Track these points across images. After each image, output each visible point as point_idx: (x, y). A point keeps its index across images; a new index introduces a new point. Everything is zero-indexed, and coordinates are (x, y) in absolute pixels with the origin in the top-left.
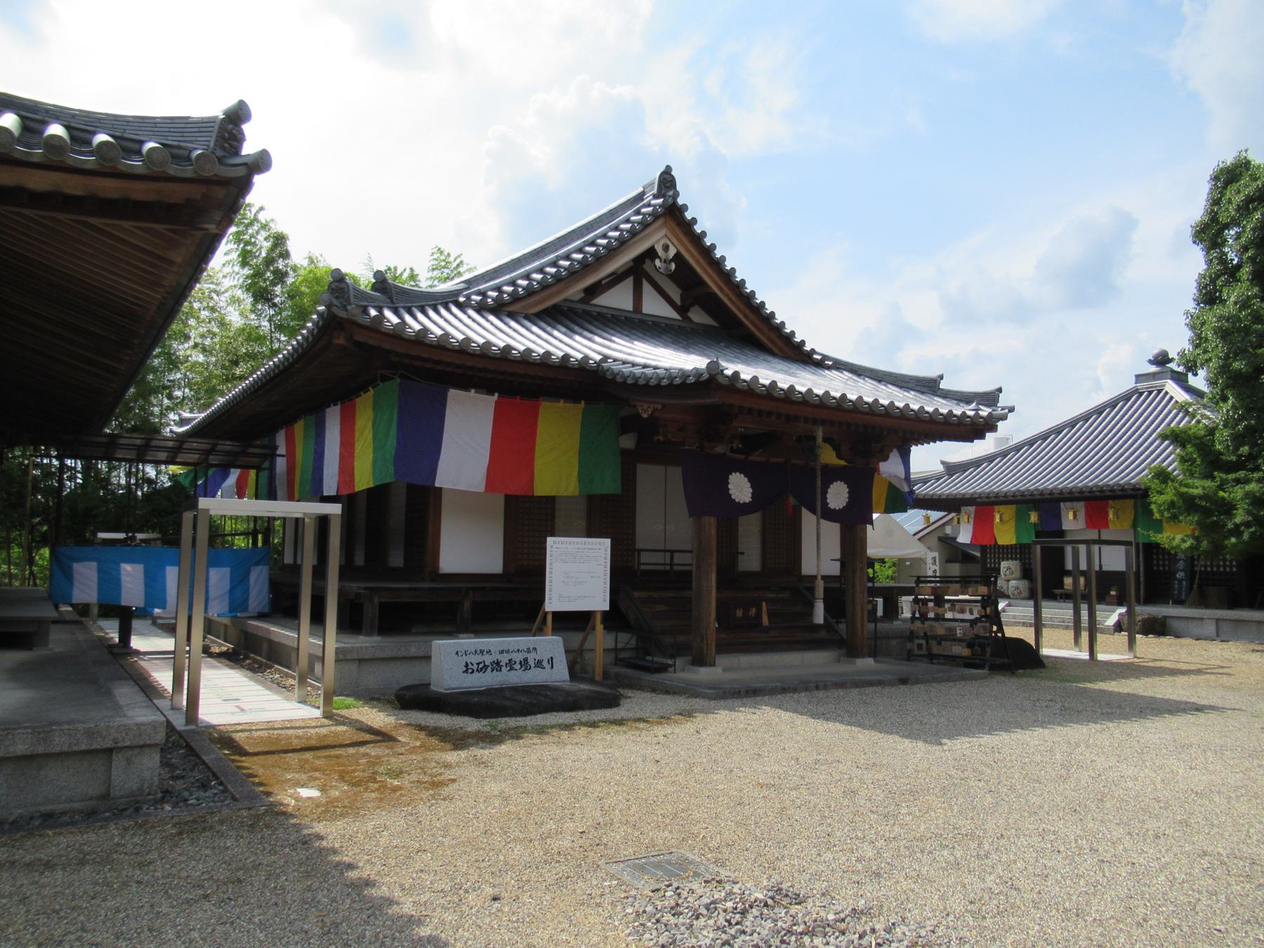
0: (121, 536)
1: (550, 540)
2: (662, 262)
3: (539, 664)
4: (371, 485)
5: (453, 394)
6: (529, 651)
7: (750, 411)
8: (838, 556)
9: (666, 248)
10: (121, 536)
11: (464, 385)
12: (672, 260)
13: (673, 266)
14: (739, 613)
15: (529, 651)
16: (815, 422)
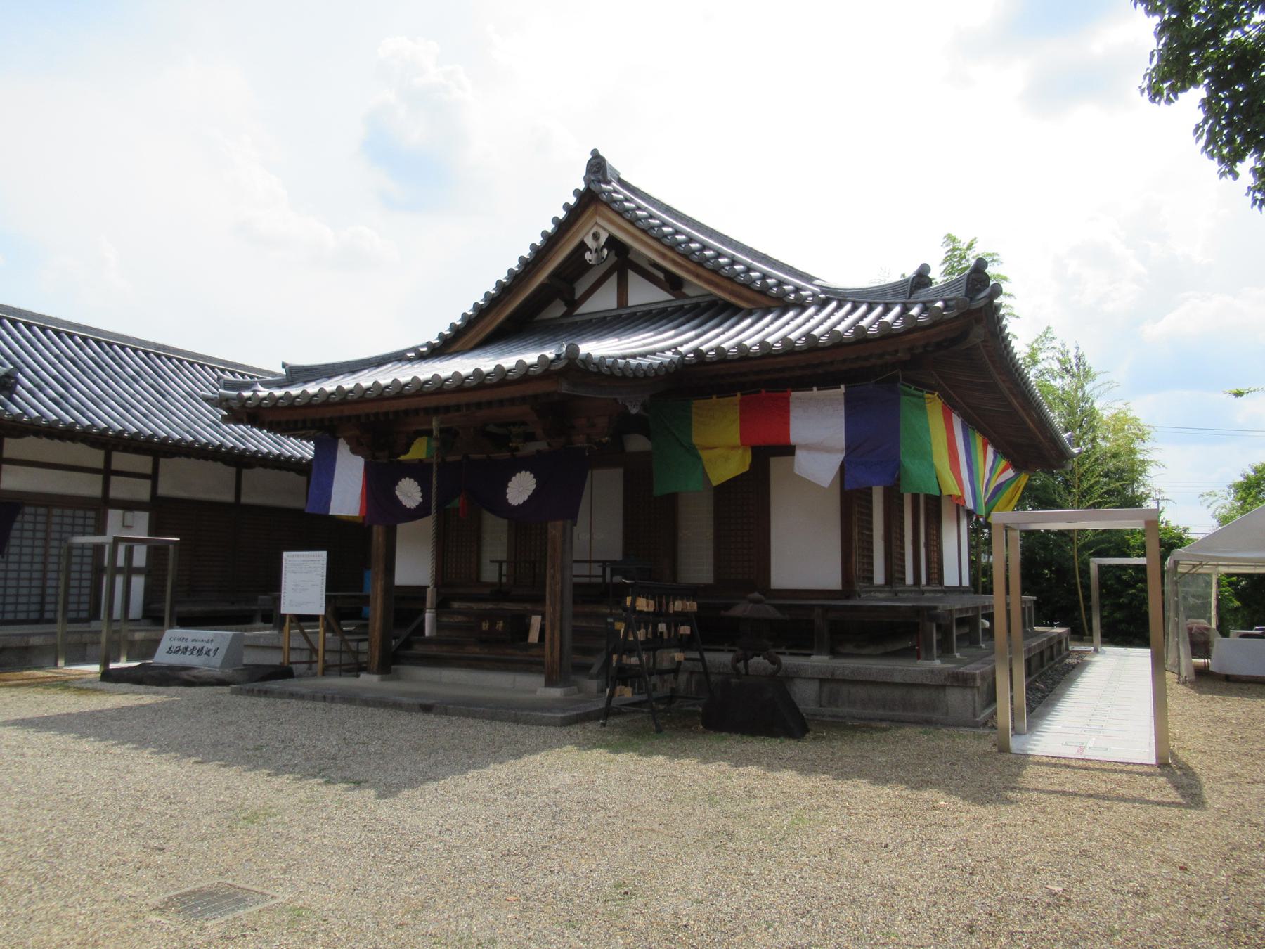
2: (602, 249)
3: (207, 653)
5: (794, 394)
9: (596, 237)
14: (485, 626)
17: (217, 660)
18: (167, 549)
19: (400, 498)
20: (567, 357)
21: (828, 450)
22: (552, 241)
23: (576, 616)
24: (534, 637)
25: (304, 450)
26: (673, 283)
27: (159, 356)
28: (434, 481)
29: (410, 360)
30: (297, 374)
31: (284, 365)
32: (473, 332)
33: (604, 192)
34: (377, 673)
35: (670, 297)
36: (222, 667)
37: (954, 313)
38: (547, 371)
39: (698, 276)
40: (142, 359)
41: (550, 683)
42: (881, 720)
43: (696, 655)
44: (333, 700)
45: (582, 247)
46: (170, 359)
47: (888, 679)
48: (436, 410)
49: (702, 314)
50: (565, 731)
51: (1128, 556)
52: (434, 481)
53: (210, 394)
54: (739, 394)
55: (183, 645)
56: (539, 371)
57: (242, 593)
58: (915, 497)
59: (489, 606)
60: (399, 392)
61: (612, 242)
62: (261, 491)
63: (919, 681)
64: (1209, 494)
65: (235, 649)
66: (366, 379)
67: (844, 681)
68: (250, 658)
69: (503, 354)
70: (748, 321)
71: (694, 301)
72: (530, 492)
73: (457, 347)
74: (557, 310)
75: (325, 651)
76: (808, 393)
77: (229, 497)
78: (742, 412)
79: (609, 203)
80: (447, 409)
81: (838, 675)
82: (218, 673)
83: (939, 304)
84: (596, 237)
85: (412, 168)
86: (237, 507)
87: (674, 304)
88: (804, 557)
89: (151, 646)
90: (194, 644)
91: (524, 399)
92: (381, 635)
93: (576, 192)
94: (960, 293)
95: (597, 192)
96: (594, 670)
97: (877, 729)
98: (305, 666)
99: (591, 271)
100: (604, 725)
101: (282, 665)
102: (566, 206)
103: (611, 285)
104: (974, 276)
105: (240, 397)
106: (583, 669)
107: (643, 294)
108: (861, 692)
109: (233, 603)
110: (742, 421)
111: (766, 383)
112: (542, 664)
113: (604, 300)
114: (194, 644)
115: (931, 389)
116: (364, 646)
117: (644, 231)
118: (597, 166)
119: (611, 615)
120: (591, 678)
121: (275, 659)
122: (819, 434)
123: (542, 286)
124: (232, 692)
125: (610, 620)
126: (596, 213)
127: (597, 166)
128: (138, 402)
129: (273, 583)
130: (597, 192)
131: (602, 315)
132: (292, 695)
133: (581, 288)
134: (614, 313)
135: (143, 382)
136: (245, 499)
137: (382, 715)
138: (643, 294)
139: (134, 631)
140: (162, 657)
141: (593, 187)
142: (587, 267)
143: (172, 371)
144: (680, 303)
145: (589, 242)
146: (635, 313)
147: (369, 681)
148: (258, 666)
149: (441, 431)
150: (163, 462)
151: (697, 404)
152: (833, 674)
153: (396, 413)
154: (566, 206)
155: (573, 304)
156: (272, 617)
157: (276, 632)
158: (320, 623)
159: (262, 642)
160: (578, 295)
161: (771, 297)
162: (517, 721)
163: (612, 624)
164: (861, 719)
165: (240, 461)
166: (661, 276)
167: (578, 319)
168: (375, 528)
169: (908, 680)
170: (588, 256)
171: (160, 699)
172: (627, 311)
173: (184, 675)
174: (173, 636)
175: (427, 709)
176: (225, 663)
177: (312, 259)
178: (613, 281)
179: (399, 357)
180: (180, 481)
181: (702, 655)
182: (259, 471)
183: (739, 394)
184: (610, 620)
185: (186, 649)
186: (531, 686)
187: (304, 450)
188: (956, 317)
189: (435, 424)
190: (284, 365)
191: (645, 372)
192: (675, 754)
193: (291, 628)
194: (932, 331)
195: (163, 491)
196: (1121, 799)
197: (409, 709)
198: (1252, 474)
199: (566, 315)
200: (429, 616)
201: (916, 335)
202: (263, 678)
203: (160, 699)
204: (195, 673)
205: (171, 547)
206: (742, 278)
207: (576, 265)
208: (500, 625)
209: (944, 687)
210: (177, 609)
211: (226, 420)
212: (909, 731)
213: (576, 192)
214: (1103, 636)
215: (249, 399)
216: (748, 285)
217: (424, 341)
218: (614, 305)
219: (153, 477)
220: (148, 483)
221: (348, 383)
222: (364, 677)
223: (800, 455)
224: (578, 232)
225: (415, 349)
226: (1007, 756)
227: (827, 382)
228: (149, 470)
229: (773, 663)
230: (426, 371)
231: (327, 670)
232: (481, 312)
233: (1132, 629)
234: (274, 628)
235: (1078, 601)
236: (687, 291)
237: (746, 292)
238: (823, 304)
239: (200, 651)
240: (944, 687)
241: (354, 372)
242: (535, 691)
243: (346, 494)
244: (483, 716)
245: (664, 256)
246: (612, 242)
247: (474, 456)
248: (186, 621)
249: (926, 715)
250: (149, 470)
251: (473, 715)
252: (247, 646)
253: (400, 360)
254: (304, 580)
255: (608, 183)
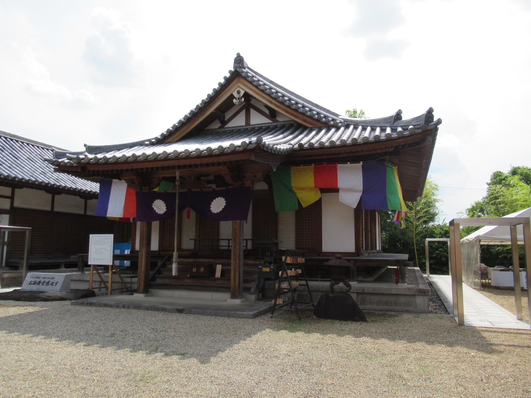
0: (6, 240)
1: (112, 236)
2: (238, 99)
3: (52, 284)
4: (122, 216)
5: (339, 165)
6: (52, 278)
7: (127, 170)
8: (194, 237)
9: (239, 92)
10: (6, 240)
11: (344, 161)
12: (242, 97)
13: (243, 99)
14: (194, 270)
15: (52, 278)
16: (174, 167)
17: (58, 287)
18: (25, 233)
19: (155, 209)
20: (256, 143)
21: (359, 191)
22: (217, 93)
23: (245, 264)
24: (218, 274)
25: (94, 187)
26: (273, 114)
27: (12, 140)
28: (177, 201)
29: (147, 145)
30: (91, 149)
31: (85, 145)
32: (178, 133)
33: (243, 72)
34: (143, 293)
35: (270, 121)
36: (61, 291)
37: (420, 131)
38: (245, 149)
39: (287, 112)
40: (4, 141)
41: (233, 297)
42: (392, 311)
43: (304, 282)
44: (128, 307)
45: (232, 97)
46: (17, 141)
47: (388, 292)
48: (179, 167)
49: (279, 130)
50: (257, 320)
51: (435, 237)
52: (177, 201)
53: (48, 158)
54: (313, 165)
55: (38, 280)
56: (241, 149)
57: (74, 255)
58: (366, 212)
59: (191, 260)
60: (146, 159)
61: (247, 96)
62: (74, 206)
63: (403, 293)
64: (460, 213)
65: (68, 280)
66: (128, 153)
67: (369, 294)
68: (75, 286)
69: (201, 143)
70: (314, 133)
71: (282, 123)
72: (223, 207)
73: (169, 140)
74: (216, 125)
75: (112, 282)
76: (299, 167)
77: (48, 208)
78: (315, 173)
79: (246, 78)
80: (184, 167)
81: (366, 291)
82: (59, 294)
83: (411, 127)
84: (239, 92)
85: (377, 7)
86: (52, 213)
87: (272, 124)
88: (338, 237)
89: (18, 282)
90: (44, 280)
91: (225, 163)
92: (145, 274)
93: (230, 71)
94: (422, 122)
95: (239, 73)
96: (252, 290)
97: (390, 316)
98: (98, 289)
99: (233, 108)
100: (272, 317)
101: (88, 290)
102: (225, 78)
103: (243, 114)
104: (428, 115)
105: (78, 158)
106: (247, 290)
107: (257, 119)
108: (376, 298)
109: (49, 259)
110: (315, 177)
111: (325, 161)
112: (229, 288)
113: (239, 121)
114: (44, 280)
115: (395, 165)
116: (135, 280)
117: (262, 91)
118: (239, 61)
119: (260, 264)
120: (251, 294)
121: (83, 286)
122: (351, 181)
123: (212, 114)
124: (72, 304)
125: (260, 267)
126: (238, 81)
127: (239, 61)
128: (5, 161)
129: (117, 249)
130: (239, 73)
131: (232, 129)
132: (106, 305)
133: (228, 116)
134: (244, 127)
135: (6, 152)
136: (56, 209)
137: (161, 315)
138: (257, 119)
139: (4, 273)
140: (25, 287)
141: (238, 70)
142: (233, 105)
143: (19, 147)
144: (275, 124)
145: (235, 94)
146: (254, 128)
147: (138, 297)
148: (77, 290)
149: (180, 177)
150: (17, 190)
151: (293, 168)
152: (363, 290)
153: (152, 168)
154: (225, 78)
155: (224, 123)
156: (84, 265)
157: (80, 273)
158: (92, 268)
159: (74, 278)
160: (227, 118)
161: (322, 122)
162: (229, 316)
163: (261, 269)
164: (381, 311)
165: (54, 191)
166: (267, 112)
167: (227, 129)
168: (139, 224)
169: (398, 293)
170: (234, 101)
171: (37, 309)
172: (250, 127)
173: (41, 295)
174: (30, 276)
175: (180, 311)
176: (62, 289)
177: (113, 94)
178: (243, 113)
179: (141, 144)
180: (25, 200)
181: (307, 282)
182: (63, 195)
183: (313, 165)
184: (260, 267)
185: (40, 282)
186: (222, 298)
187: (94, 187)
188: (420, 133)
189: (177, 174)
190: (85, 145)
191: (281, 152)
192: (324, 332)
193: (93, 270)
194: (409, 138)
195: (17, 204)
196: (502, 345)
197: (171, 311)
198: (475, 205)
199: (220, 128)
200: (174, 266)
201: (401, 140)
202: (84, 296)
203: (37, 309)
204: (47, 294)
205: (27, 232)
206: (309, 113)
207: (229, 103)
208: (203, 269)
209: (415, 295)
210: (29, 262)
211: (56, 170)
212: (406, 316)
213: (230, 71)
214: (430, 271)
215: (83, 159)
216: (311, 117)
217: (155, 136)
218: (244, 124)
219: (12, 198)
220: (9, 200)
221: (109, 155)
222: (136, 295)
223: (341, 193)
224: (230, 89)
225: (149, 140)
226: (463, 327)
227: (354, 160)
228: (9, 194)
229: (347, 286)
230: (159, 150)
231: (113, 292)
232: (183, 124)
233: (437, 267)
234: (79, 271)
235: (415, 256)
236: (278, 119)
237: (310, 120)
238: (347, 127)
239: (48, 283)
240: (415, 295)
241: (119, 150)
242: (226, 301)
243: (116, 207)
244: (211, 314)
245: (271, 102)
246: (247, 96)
247: (193, 190)
248: (32, 268)
249: (406, 308)
250: (9, 194)
251: (203, 314)
252: (72, 280)
253: (141, 145)
254: (101, 249)
255: (244, 68)
